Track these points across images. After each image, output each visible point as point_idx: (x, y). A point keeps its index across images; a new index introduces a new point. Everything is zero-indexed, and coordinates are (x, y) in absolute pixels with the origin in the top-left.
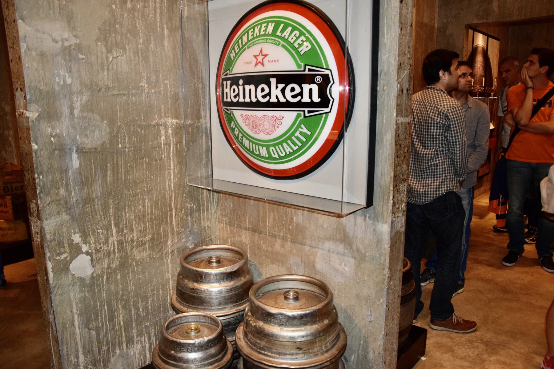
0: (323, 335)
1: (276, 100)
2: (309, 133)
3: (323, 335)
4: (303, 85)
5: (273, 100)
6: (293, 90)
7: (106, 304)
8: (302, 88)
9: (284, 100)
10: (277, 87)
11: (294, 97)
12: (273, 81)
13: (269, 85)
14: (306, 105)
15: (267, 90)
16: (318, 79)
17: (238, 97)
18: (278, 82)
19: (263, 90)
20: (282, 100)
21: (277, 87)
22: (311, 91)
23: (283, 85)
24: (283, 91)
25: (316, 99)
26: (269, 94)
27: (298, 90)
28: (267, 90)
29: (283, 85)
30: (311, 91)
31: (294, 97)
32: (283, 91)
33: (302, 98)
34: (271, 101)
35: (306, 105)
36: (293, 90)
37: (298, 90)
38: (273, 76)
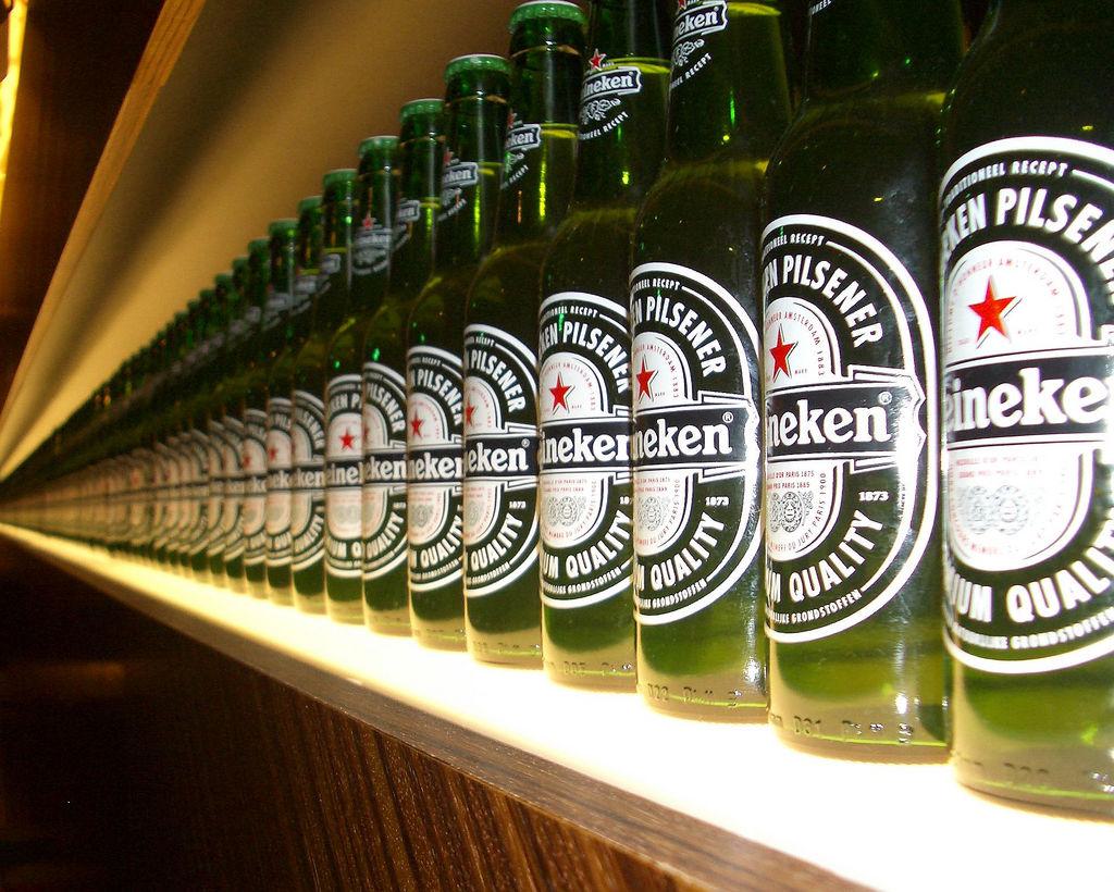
0: (278, 354)
1: (581, 460)
2: (877, 526)
3: (278, 354)
4: (705, 428)
5: (804, 440)
6: (838, 419)
7: (940, 196)
8: (703, 433)
9: (823, 440)
10: (809, 417)
11: (691, 446)
12: (577, 432)
13: (1019, 383)
14: (710, 458)
15: (793, 424)
16: (728, 417)
17: (796, 436)
18: (584, 434)
19: (565, 446)
20: (674, 453)
21: (809, 417)
22: (716, 436)
23: (591, 437)
24: (591, 446)
25: (725, 449)
26: (797, 430)
27: (697, 436)
28: (793, 424)
29: (821, 411)
30: (716, 436)
31: (691, 446)
32: (591, 446)
33: (854, 435)
34: (800, 442)
35: (710, 458)
36: (838, 419)
37: (847, 419)
38: (480, 440)
